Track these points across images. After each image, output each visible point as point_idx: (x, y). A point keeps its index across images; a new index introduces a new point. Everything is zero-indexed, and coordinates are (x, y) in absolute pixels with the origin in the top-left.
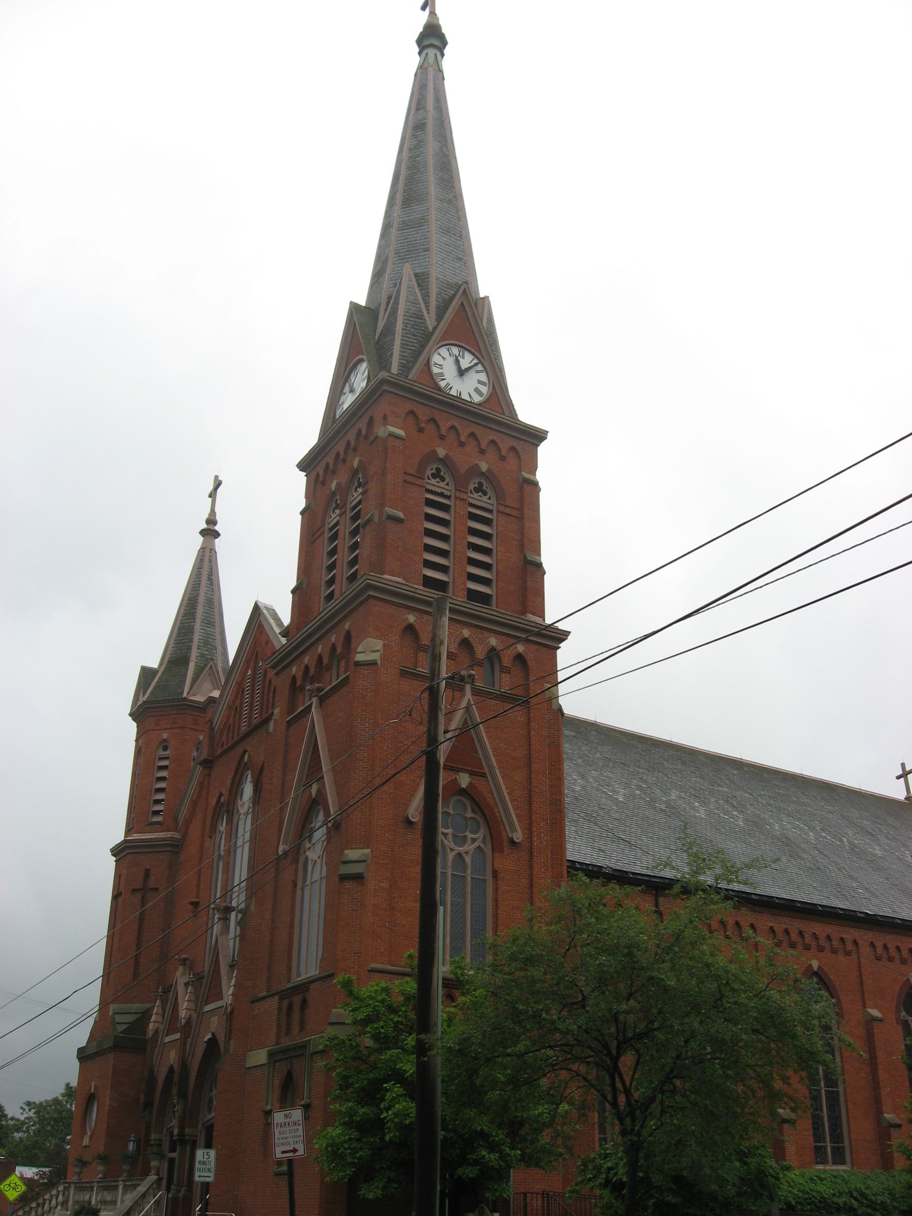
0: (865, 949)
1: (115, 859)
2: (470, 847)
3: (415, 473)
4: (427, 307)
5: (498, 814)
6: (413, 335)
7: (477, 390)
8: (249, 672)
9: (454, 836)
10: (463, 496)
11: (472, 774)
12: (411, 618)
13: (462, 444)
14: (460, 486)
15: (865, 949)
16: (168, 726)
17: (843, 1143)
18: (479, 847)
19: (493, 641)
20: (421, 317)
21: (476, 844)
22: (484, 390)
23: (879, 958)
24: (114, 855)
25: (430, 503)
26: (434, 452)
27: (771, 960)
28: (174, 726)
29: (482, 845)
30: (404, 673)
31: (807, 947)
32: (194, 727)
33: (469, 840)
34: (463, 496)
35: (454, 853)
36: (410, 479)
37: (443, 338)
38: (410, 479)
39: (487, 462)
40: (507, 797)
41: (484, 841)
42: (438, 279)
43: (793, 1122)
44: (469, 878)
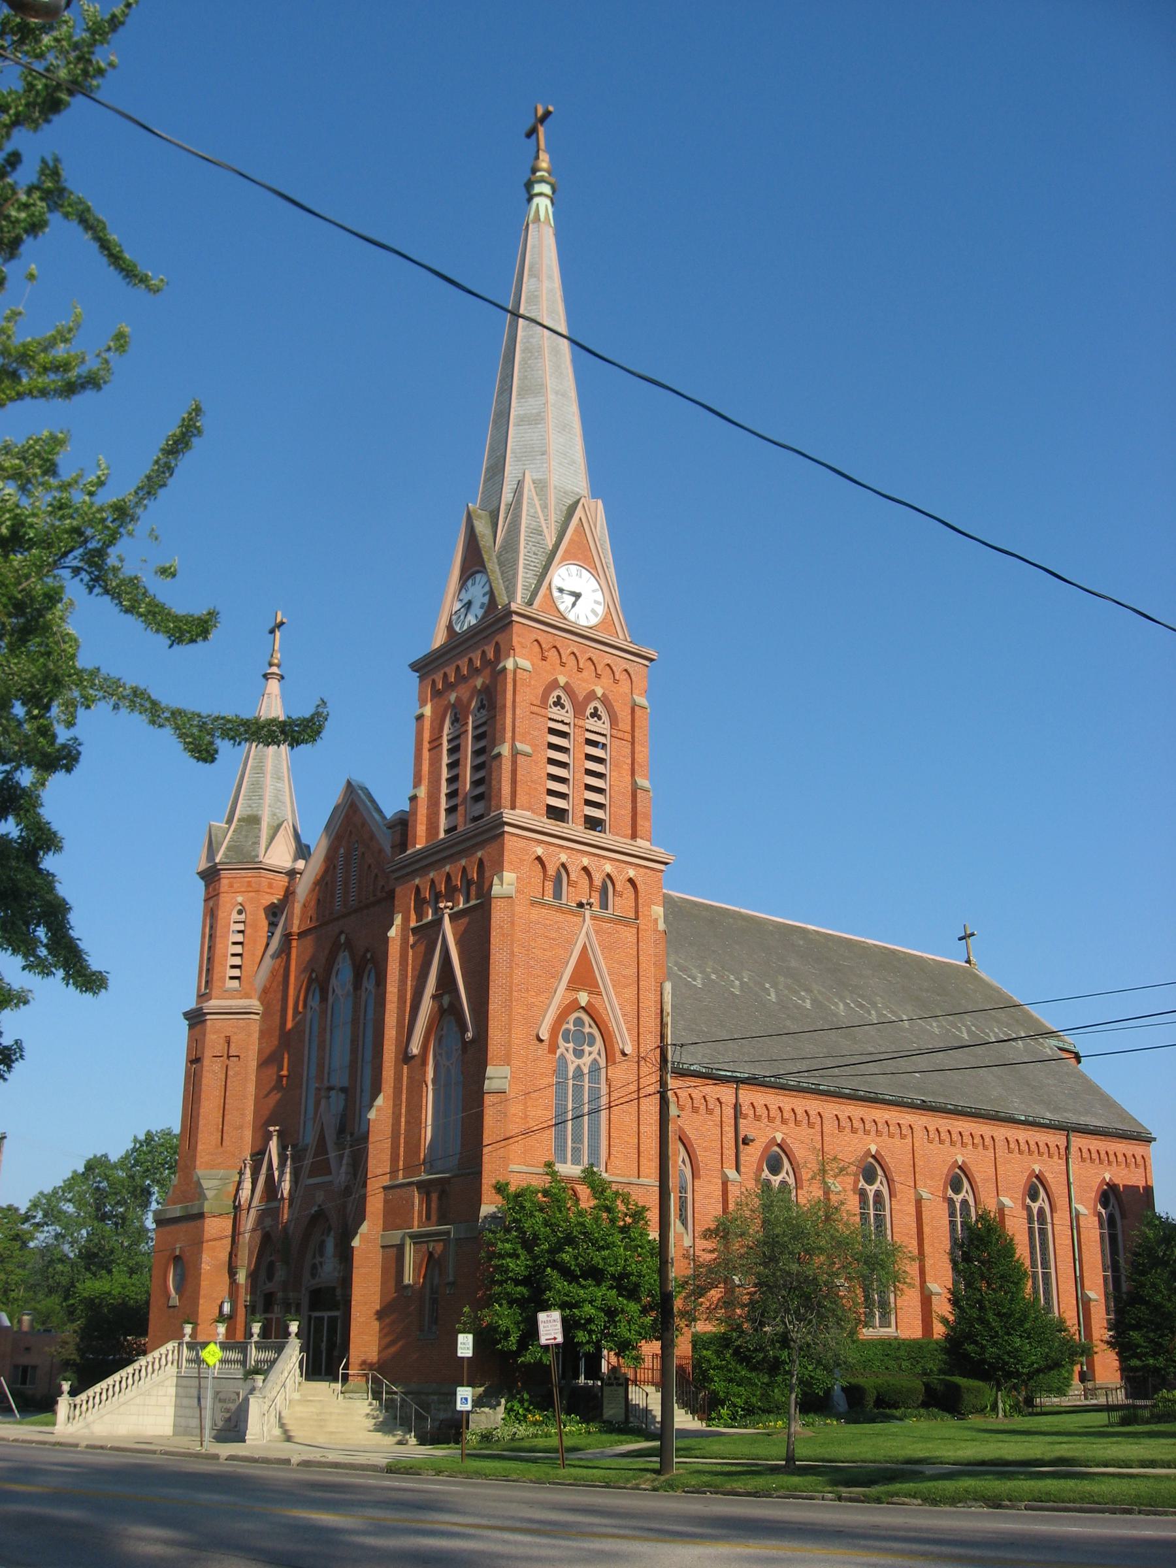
0: (919, 1133)
1: (187, 1022)
2: (586, 1060)
3: (539, 704)
4: (545, 507)
5: (611, 1029)
6: (535, 554)
7: (594, 612)
8: (342, 851)
9: (575, 1050)
10: (581, 723)
11: (590, 993)
12: (540, 851)
13: (580, 670)
14: (579, 711)
15: (919, 1133)
16: (243, 890)
17: (884, 1211)
18: (595, 1060)
19: (608, 868)
20: (540, 533)
21: (593, 1056)
22: (600, 610)
23: (930, 1141)
24: (187, 1019)
25: (552, 731)
26: (556, 681)
27: (865, 1277)
28: (251, 889)
29: (598, 1057)
30: (533, 903)
31: (866, 1132)
32: (269, 891)
33: (586, 1053)
34: (581, 723)
35: (575, 1065)
36: (535, 709)
37: (563, 559)
38: (535, 709)
39: (602, 687)
40: (619, 1013)
41: (599, 1054)
42: (555, 488)
43: (156, 289)
44: (587, 1087)
